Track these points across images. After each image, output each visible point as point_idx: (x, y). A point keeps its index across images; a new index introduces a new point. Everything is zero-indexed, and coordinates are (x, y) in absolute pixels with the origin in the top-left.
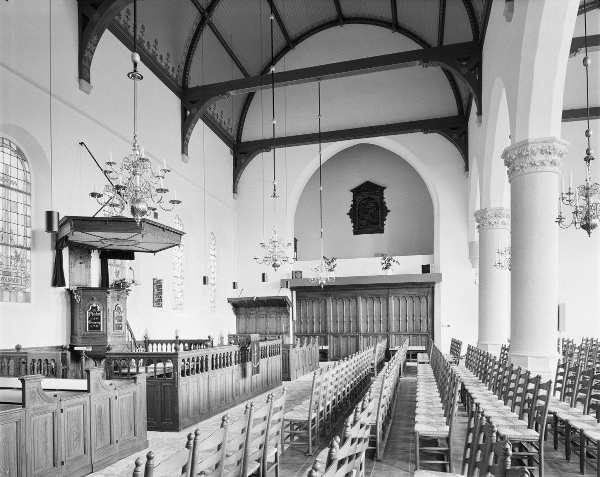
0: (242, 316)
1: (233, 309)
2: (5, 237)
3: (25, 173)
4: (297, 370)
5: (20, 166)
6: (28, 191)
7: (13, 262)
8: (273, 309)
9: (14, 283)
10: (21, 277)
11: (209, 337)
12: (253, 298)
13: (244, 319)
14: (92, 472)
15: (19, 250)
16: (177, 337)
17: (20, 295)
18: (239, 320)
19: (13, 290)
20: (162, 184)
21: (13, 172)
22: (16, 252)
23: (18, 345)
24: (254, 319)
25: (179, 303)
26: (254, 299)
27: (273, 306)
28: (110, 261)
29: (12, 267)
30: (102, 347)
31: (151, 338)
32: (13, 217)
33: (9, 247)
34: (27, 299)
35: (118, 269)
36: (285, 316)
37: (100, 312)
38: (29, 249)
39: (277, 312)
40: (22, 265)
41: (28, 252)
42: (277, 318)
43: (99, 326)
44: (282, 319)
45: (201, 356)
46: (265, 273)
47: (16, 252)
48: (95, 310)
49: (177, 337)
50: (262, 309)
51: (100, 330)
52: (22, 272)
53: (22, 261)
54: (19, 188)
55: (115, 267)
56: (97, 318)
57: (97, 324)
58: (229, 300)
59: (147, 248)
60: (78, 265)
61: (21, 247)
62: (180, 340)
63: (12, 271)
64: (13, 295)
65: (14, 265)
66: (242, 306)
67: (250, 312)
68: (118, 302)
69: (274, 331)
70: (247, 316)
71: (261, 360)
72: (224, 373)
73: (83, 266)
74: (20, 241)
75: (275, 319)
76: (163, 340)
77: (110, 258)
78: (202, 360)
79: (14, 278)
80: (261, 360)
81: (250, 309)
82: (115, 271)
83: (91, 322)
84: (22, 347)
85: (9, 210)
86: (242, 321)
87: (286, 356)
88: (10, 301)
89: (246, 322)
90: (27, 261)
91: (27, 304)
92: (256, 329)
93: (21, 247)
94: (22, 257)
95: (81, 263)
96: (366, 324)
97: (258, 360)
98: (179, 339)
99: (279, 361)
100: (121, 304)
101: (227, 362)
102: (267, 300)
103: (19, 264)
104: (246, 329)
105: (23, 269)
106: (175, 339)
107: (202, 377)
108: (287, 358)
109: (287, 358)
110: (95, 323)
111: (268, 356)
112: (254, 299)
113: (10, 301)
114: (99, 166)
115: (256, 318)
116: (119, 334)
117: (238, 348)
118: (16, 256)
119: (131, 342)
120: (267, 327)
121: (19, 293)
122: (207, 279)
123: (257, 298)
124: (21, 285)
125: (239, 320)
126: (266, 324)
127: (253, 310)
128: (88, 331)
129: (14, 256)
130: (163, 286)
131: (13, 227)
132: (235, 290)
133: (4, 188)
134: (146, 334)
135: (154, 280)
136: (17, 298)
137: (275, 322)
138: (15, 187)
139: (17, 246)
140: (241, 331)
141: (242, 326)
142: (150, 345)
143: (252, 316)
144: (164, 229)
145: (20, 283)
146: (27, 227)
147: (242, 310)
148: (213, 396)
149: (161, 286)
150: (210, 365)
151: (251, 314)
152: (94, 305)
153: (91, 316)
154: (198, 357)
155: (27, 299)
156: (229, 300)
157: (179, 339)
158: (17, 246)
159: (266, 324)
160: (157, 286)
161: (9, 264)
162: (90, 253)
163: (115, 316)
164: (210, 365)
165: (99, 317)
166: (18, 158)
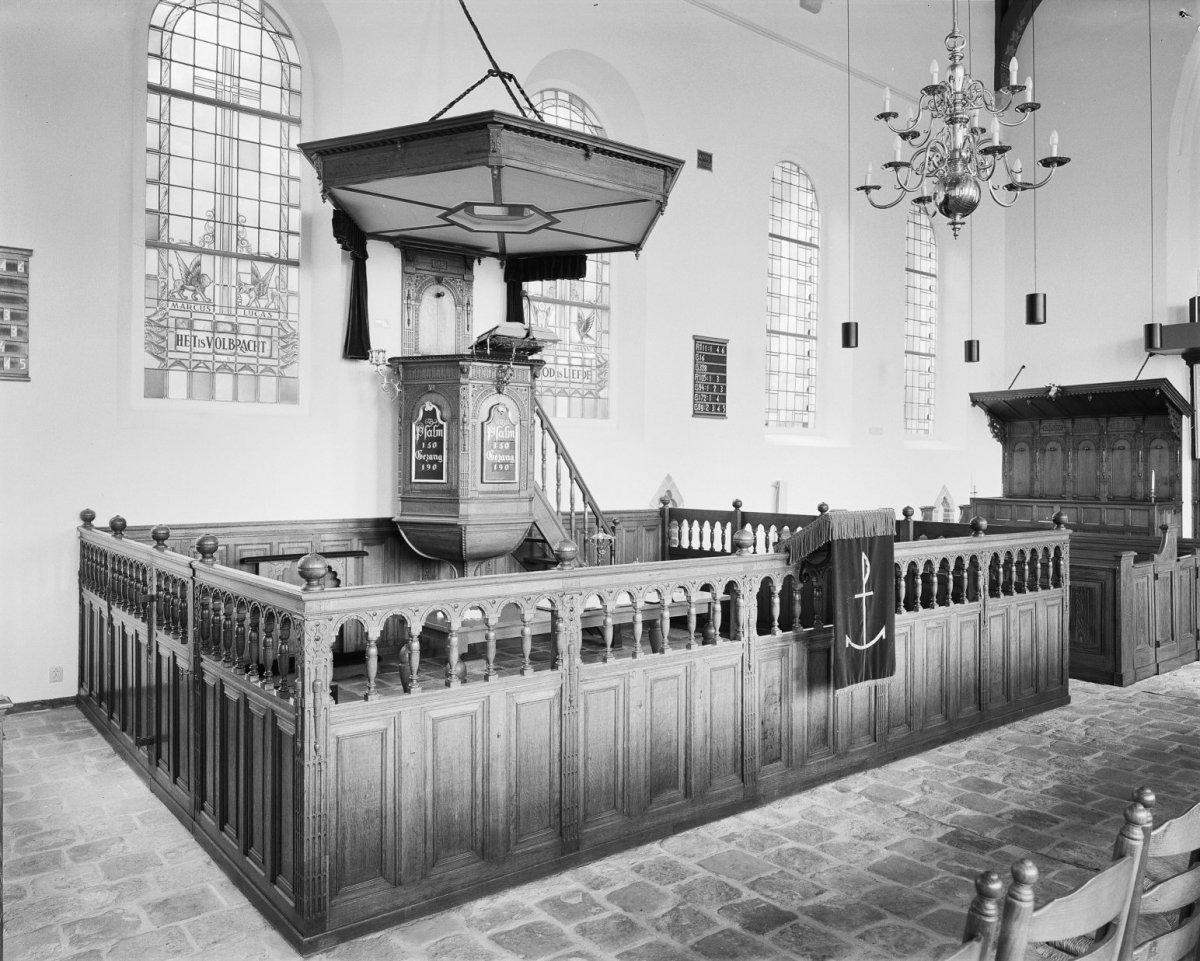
0: (1023, 445)
1: (991, 425)
2: (222, 233)
3: (286, 67)
4: (1158, 644)
5: (270, 49)
6: (295, 114)
7: (245, 299)
8: (1122, 423)
9: (249, 353)
10: (270, 337)
11: (821, 509)
12: (1048, 389)
13: (1027, 455)
14: (1158, 674)
15: (263, 268)
16: (737, 505)
17: (268, 384)
18: (1011, 456)
19: (245, 372)
20: (899, 153)
21: (249, 66)
22: (254, 272)
23: (118, 519)
24: (1059, 455)
25: (800, 406)
26: (1052, 393)
27: (1121, 412)
28: (532, 287)
29: (241, 312)
30: (445, 530)
31: (687, 504)
32: (247, 183)
33: (234, 260)
34: (288, 396)
35: (587, 313)
36: (1164, 444)
37: (441, 427)
38: (296, 264)
39: (1137, 431)
40: (272, 306)
41: (293, 271)
42: (1134, 449)
43: (440, 466)
44: (1155, 453)
45: (1054, 545)
46: (1040, 291)
47: (254, 272)
48: (430, 421)
49: (737, 505)
50: (1085, 422)
51: (514, 479)
52: (275, 323)
53: (273, 296)
54: (265, 107)
55: (575, 310)
56: (435, 445)
57: (436, 462)
58: (976, 400)
59: (621, 239)
60: (428, 297)
61: (270, 260)
62: (743, 514)
63: (240, 320)
64: (245, 381)
65: (248, 307)
66: (1020, 416)
67: (1045, 433)
68: (502, 399)
69: (1123, 491)
70: (1037, 445)
71: (903, 620)
72: (681, 671)
73: (448, 300)
74: (270, 245)
75: (1127, 453)
76: (715, 512)
77: (527, 280)
78: (1009, 561)
79: (247, 339)
80: (903, 620)
81: (1046, 423)
82: (575, 319)
83: (421, 457)
84: (128, 524)
85: (235, 166)
86: (1021, 461)
87: (1103, 588)
88: (235, 398)
89: (1033, 462)
90: (292, 294)
91: (285, 408)
92: (1064, 483)
93: (270, 260)
94: (272, 284)
95: (439, 295)
96: (470, 323)
97: (882, 617)
98: (742, 509)
99: (1055, 612)
100: (509, 403)
101: (1045, 574)
102: (1094, 395)
103: (263, 303)
104: (1032, 481)
105: (275, 315)
106: (733, 509)
107: (536, 687)
108: (1109, 596)
109: (1109, 596)
110: (431, 457)
111: (984, 593)
112: (1052, 393)
113: (235, 398)
114: (472, 23)
115: (1063, 450)
116: (501, 493)
117: (779, 565)
118: (254, 283)
119: (583, 514)
120: (1100, 480)
121: (171, 374)
122: (853, 328)
123: (1063, 390)
124: (270, 357)
125: (1011, 456)
126: (1098, 468)
127: (1051, 428)
128: (413, 480)
129: (249, 281)
130: (728, 359)
131: (248, 210)
132: (971, 364)
133: (219, 109)
134: (669, 491)
135: (696, 340)
136: (257, 391)
137: (1128, 465)
138: (255, 105)
139: (258, 258)
140: (1016, 489)
141: (1021, 472)
142: (748, 527)
143: (1052, 445)
144: (585, 147)
145: (267, 354)
146: (290, 206)
147: (1023, 428)
148: (524, 801)
149: (723, 359)
150: (983, 580)
151: (1049, 439)
152: (429, 407)
153: (421, 439)
154: (1034, 551)
155: (288, 396)
156: (976, 400)
157: (742, 509)
158: (258, 258)
159: (1098, 468)
160: (708, 358)
161: (234, 305)
162: (469, 268)
163: (488, 438)
164: (983, 580)
165: (440, 440)
166: (262, 28)
